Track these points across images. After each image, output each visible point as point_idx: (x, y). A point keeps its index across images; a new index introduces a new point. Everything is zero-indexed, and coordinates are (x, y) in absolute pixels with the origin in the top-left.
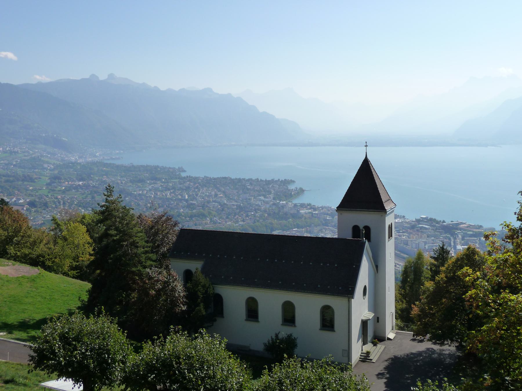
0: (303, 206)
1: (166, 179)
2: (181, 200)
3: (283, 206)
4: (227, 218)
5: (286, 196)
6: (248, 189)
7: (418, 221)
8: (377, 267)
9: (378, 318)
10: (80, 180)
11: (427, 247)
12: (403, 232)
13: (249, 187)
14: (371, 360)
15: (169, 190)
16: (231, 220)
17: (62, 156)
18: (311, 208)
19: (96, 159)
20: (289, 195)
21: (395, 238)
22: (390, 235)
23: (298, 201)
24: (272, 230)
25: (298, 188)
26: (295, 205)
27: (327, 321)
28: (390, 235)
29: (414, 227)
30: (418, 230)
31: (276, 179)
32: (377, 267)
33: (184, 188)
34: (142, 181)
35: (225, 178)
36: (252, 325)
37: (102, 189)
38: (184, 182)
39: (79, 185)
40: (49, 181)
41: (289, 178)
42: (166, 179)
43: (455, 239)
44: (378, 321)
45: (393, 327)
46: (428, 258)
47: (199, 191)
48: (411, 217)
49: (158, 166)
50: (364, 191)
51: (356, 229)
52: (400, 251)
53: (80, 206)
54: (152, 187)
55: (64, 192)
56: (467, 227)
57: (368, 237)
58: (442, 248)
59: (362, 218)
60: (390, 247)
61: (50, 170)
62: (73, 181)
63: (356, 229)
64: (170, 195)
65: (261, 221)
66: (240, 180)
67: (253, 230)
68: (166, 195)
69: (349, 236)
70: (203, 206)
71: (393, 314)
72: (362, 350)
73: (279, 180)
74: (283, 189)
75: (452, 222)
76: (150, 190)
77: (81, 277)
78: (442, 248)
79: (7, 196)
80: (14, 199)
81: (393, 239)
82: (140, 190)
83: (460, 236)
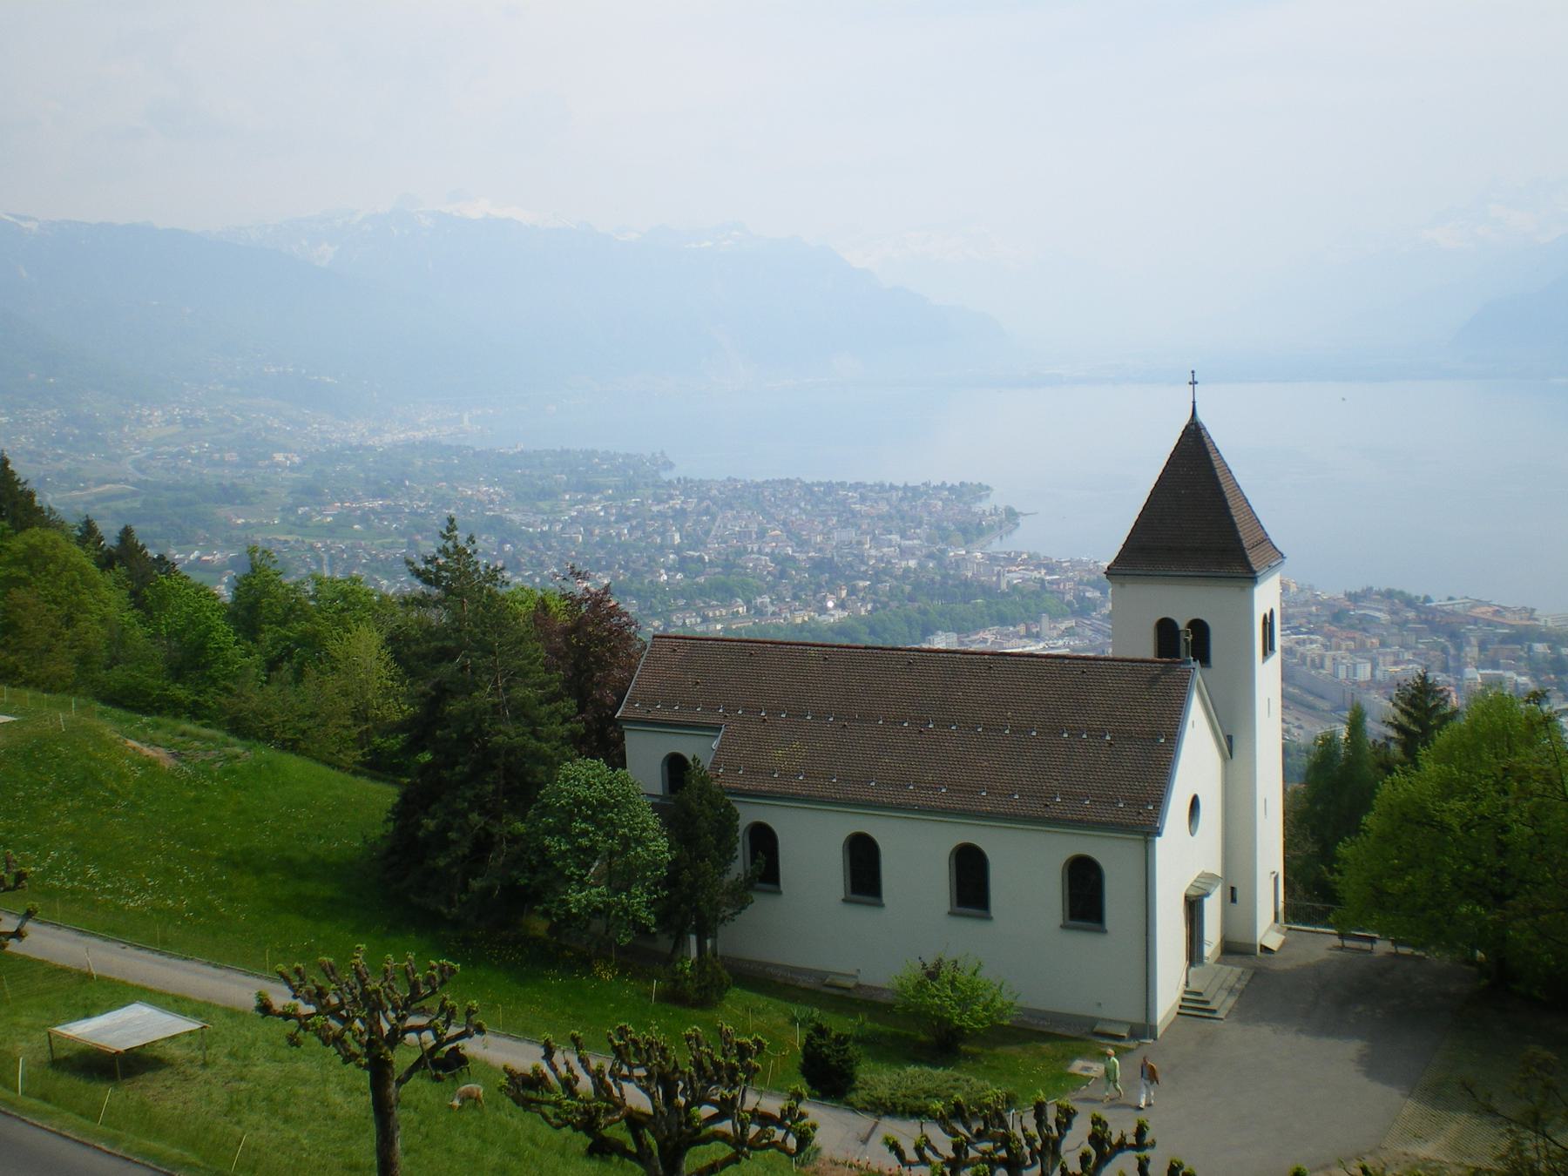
0: (1011, 560)
1: (616, 488)
2: (661, 549)
3: (959, 563)
4: (795, 597)
5: (964, 532)
6: (854, 514)
7: (1353, 598)
8: (1230, 739)
9: (1233, 889)
10: (375, 496)
11: (1374, 675)
12: (1310, 632)
13: (857, 507)
14: (1214, 1011)
15: (627, 519)
16: (806, 605)
17: (324, 428)
18: (1038, 567)
19: (420, 435)
20: (972, 531)
21: (1285, 651)
22: (1268, 647)
23: (997, 546)
24: (928, 631)
25: (1001, 507)
26: (993, 559)
27: (1085, 894)
28: (1268, 647)
29: (1341, 618)
30: (1352, 627)
31: (936, 482)
32: (1230, 739)
33: (670, 513)
34: (547, 494)
35: (788, 482)
36: (862, 917)
37: (437, 522)
38: (671, 497)
39: (372, 510)
40: (290, 500)
41: (972, 478)
42: (616, 488)
43: (1459, 648)
44: (1234, 900)
45: (1276, 914)
46: (1381, 714)
47: (714, 519)
48: (1332, 589)
49: (594, 453)
50: (1193, 520)
51: (1166, 629)
52: (1300, 687)
53: (377, 570)
54: (580, 512)
55: (331, 530)
56: (1497, 612)
57: (1201, 651)
58: (1424, 678)
59: (1183, 601)
60: (1267, 678)
61: (292, 469)
62: (356, 499)
63: (1166, 629)
64: (630, 534)
65: (894, 604)
66: (830, 488)
67: (873, 632)
68: (619, 535)
69: (1146, 648)
70: (728, 566)
71: (1276, 879)
72: (1187, 984)
73: (944, 484)
74: (962, 514)
75: (1450, 599)
76: (574, 520)
77: (377, 766)
78: (1424, 678)
79: (178, 544)
80: (196, 553)
81: (1276, 658)
82: (543, 522)
83: (1474, 641)
